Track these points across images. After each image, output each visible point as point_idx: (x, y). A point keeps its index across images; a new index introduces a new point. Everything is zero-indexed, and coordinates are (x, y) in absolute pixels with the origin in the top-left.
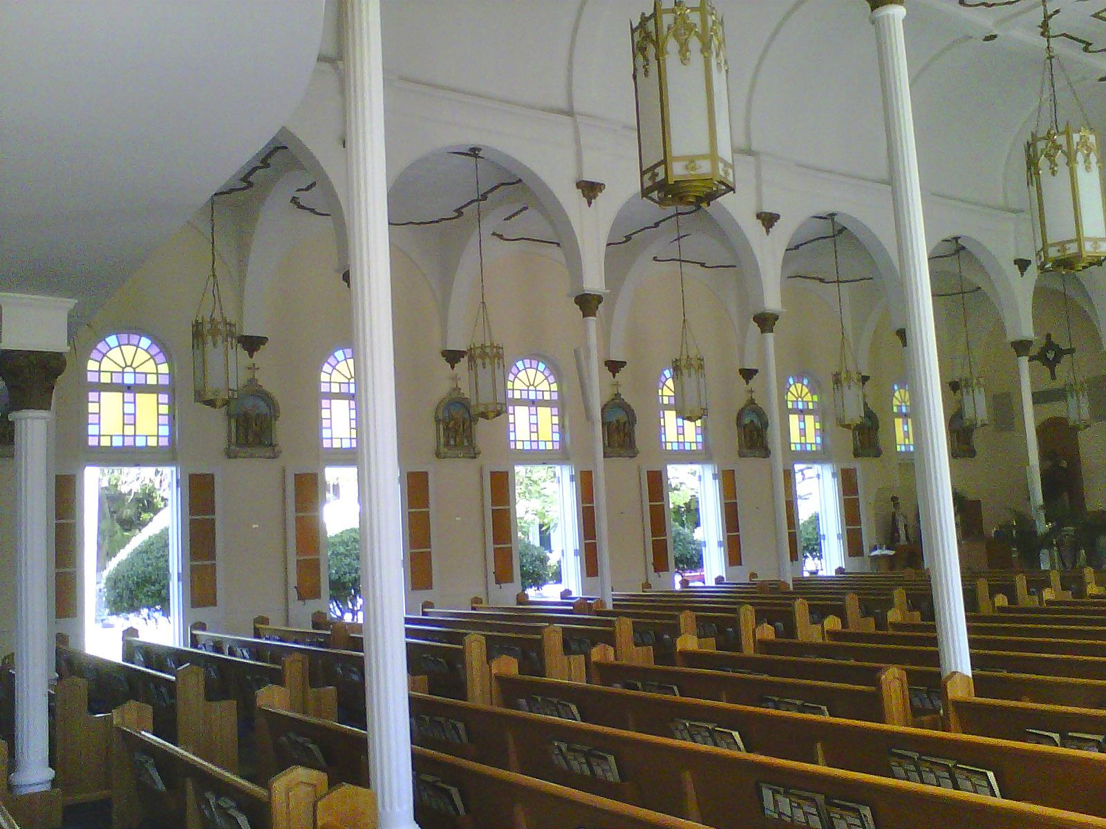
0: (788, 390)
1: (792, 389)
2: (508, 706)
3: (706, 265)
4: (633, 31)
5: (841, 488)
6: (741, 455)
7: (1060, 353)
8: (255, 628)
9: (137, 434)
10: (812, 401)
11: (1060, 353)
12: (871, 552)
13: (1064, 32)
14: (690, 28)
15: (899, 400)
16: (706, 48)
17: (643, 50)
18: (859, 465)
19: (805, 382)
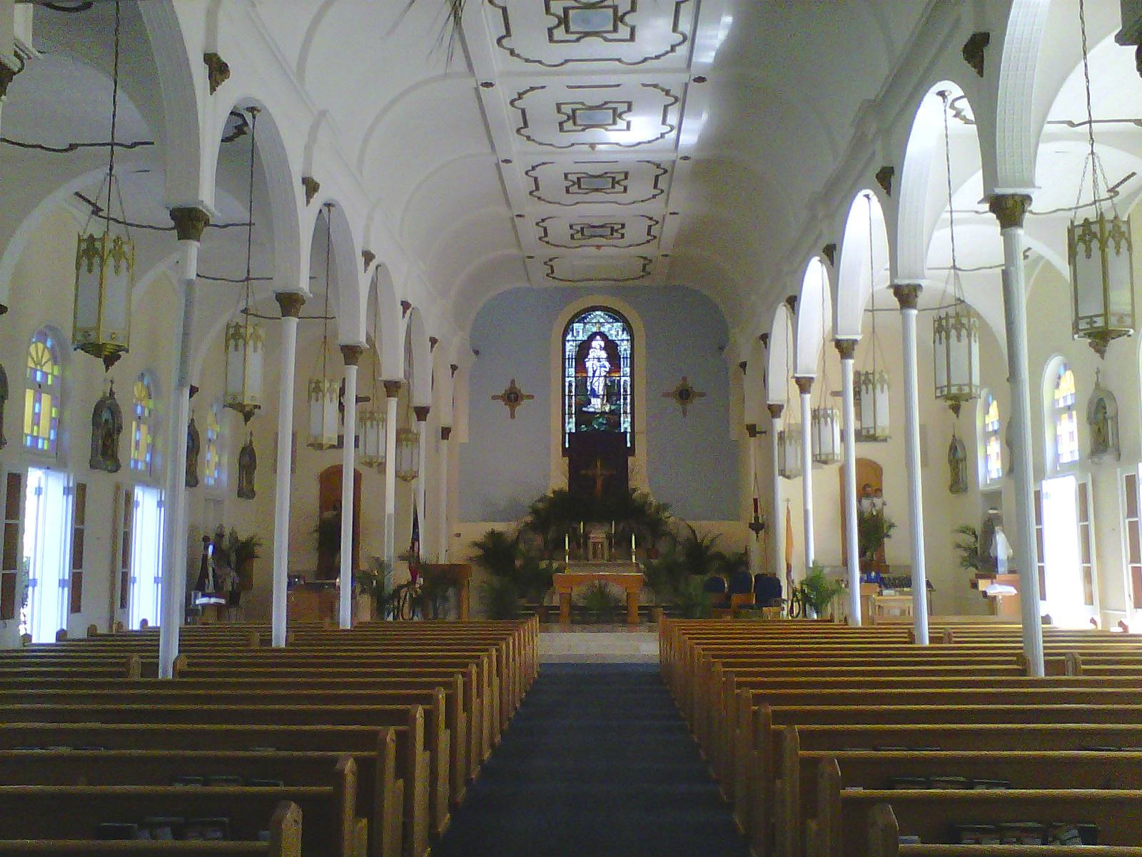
3: (91, 208)
4: (934, 321)
5: (21, 504)
6: (93, 466)
10: (52, 374)
13: (605, 43)
14: (963, 325)
15: (34, 362)
16: (969, 336)
17: (940, 333)
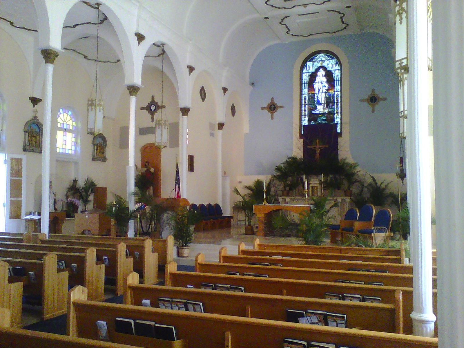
0: (59, 116)
1: (61, 116)
2: (135, 304)
7: (157, 107)
8: (126, 250)
9: (71, 149)
11: (157, 107)
12: (26, 215)
18: (24, 157)
19: (70, 113)
